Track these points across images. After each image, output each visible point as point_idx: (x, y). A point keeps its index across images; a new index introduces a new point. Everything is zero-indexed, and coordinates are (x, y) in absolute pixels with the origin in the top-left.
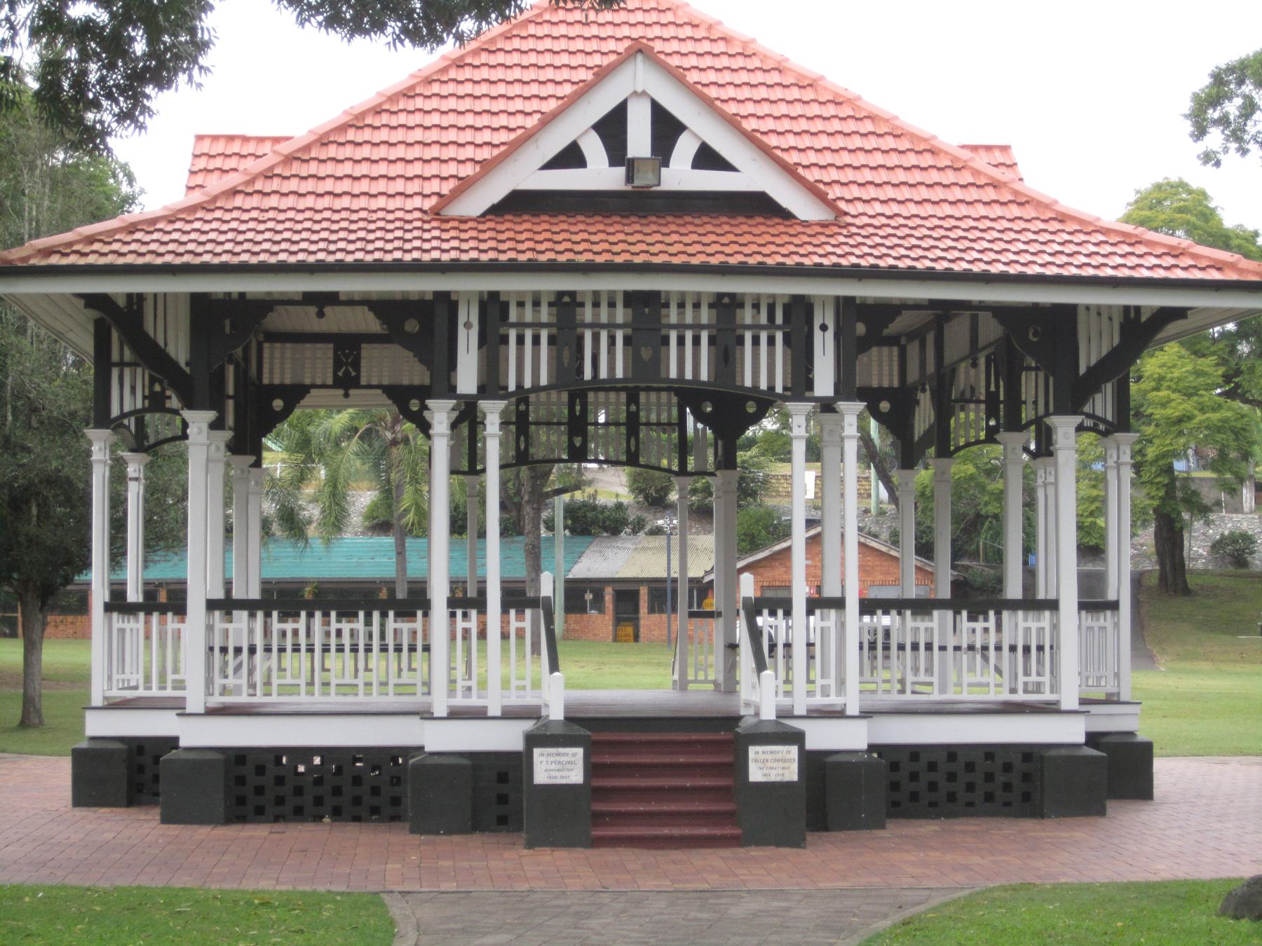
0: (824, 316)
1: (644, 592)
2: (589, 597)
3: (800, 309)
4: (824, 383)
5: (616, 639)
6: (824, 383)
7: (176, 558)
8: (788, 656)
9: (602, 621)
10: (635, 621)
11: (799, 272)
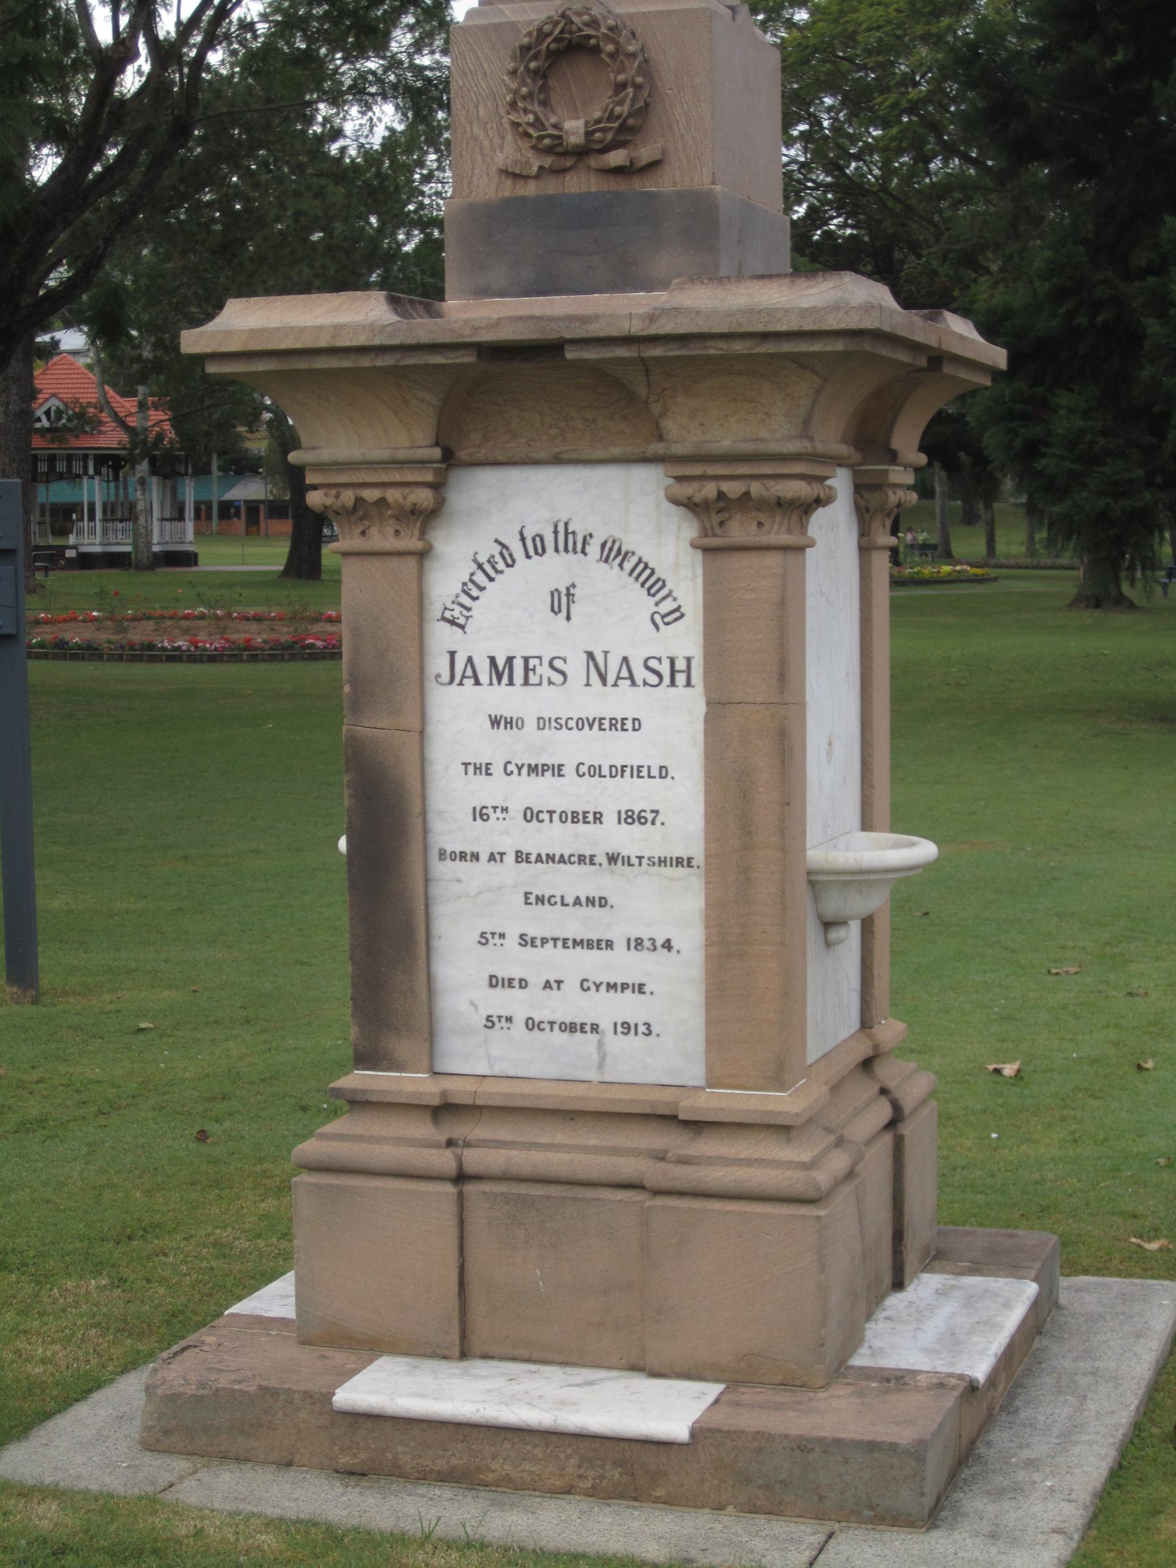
0: (91, 457)
1: (262, 507)
2: (232, 510)
3: (86, 457)
4: (91, 472)
5: (247, 534)
6: (91, 472)
7: (341, 1490)
8: (92, 518)
9: (240, 524)
10: (257, 523)
11: (87, 448)
